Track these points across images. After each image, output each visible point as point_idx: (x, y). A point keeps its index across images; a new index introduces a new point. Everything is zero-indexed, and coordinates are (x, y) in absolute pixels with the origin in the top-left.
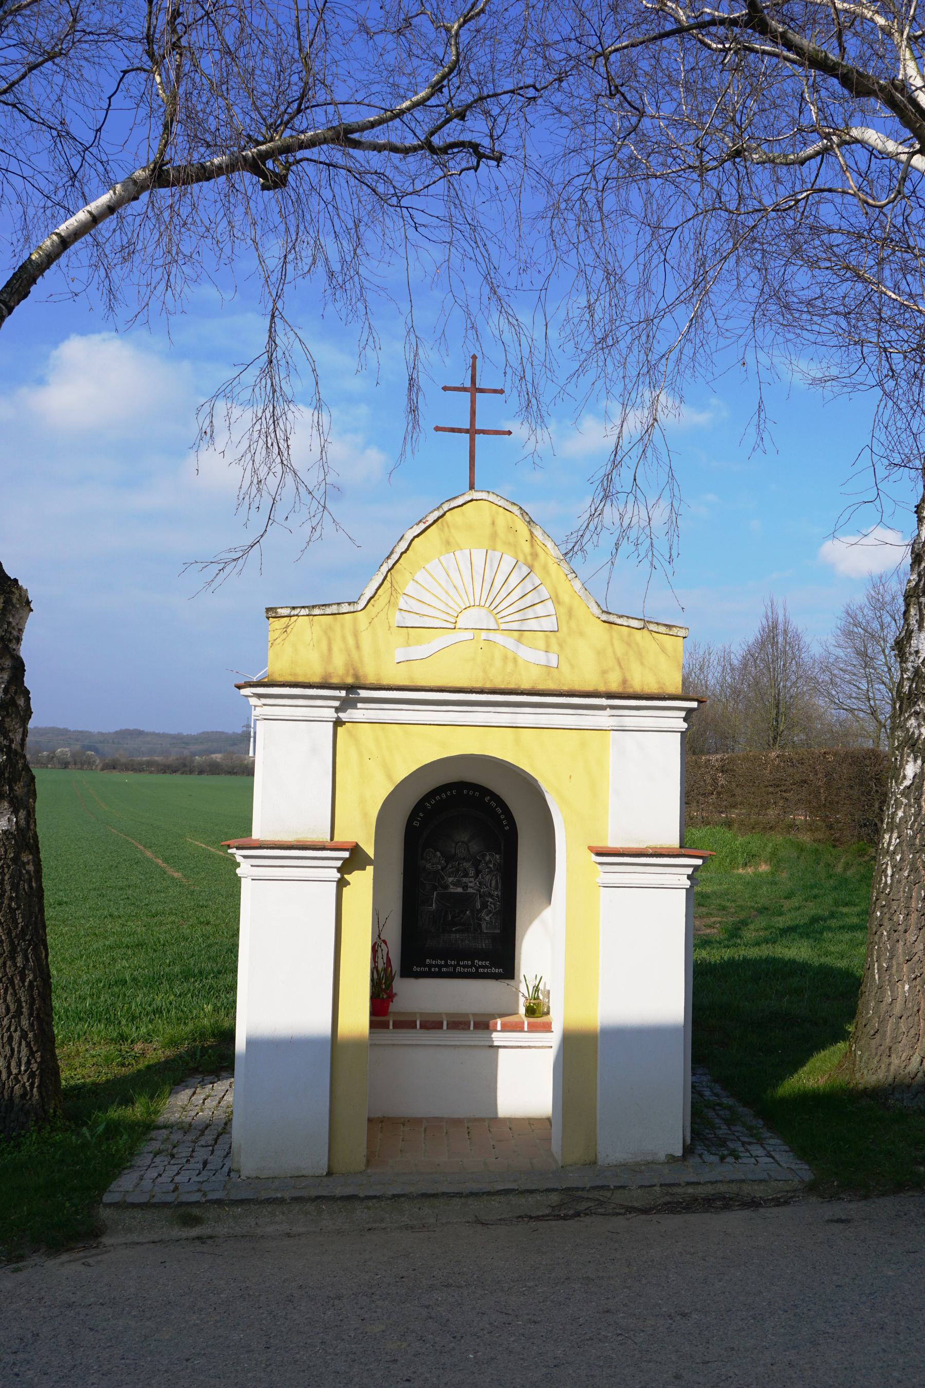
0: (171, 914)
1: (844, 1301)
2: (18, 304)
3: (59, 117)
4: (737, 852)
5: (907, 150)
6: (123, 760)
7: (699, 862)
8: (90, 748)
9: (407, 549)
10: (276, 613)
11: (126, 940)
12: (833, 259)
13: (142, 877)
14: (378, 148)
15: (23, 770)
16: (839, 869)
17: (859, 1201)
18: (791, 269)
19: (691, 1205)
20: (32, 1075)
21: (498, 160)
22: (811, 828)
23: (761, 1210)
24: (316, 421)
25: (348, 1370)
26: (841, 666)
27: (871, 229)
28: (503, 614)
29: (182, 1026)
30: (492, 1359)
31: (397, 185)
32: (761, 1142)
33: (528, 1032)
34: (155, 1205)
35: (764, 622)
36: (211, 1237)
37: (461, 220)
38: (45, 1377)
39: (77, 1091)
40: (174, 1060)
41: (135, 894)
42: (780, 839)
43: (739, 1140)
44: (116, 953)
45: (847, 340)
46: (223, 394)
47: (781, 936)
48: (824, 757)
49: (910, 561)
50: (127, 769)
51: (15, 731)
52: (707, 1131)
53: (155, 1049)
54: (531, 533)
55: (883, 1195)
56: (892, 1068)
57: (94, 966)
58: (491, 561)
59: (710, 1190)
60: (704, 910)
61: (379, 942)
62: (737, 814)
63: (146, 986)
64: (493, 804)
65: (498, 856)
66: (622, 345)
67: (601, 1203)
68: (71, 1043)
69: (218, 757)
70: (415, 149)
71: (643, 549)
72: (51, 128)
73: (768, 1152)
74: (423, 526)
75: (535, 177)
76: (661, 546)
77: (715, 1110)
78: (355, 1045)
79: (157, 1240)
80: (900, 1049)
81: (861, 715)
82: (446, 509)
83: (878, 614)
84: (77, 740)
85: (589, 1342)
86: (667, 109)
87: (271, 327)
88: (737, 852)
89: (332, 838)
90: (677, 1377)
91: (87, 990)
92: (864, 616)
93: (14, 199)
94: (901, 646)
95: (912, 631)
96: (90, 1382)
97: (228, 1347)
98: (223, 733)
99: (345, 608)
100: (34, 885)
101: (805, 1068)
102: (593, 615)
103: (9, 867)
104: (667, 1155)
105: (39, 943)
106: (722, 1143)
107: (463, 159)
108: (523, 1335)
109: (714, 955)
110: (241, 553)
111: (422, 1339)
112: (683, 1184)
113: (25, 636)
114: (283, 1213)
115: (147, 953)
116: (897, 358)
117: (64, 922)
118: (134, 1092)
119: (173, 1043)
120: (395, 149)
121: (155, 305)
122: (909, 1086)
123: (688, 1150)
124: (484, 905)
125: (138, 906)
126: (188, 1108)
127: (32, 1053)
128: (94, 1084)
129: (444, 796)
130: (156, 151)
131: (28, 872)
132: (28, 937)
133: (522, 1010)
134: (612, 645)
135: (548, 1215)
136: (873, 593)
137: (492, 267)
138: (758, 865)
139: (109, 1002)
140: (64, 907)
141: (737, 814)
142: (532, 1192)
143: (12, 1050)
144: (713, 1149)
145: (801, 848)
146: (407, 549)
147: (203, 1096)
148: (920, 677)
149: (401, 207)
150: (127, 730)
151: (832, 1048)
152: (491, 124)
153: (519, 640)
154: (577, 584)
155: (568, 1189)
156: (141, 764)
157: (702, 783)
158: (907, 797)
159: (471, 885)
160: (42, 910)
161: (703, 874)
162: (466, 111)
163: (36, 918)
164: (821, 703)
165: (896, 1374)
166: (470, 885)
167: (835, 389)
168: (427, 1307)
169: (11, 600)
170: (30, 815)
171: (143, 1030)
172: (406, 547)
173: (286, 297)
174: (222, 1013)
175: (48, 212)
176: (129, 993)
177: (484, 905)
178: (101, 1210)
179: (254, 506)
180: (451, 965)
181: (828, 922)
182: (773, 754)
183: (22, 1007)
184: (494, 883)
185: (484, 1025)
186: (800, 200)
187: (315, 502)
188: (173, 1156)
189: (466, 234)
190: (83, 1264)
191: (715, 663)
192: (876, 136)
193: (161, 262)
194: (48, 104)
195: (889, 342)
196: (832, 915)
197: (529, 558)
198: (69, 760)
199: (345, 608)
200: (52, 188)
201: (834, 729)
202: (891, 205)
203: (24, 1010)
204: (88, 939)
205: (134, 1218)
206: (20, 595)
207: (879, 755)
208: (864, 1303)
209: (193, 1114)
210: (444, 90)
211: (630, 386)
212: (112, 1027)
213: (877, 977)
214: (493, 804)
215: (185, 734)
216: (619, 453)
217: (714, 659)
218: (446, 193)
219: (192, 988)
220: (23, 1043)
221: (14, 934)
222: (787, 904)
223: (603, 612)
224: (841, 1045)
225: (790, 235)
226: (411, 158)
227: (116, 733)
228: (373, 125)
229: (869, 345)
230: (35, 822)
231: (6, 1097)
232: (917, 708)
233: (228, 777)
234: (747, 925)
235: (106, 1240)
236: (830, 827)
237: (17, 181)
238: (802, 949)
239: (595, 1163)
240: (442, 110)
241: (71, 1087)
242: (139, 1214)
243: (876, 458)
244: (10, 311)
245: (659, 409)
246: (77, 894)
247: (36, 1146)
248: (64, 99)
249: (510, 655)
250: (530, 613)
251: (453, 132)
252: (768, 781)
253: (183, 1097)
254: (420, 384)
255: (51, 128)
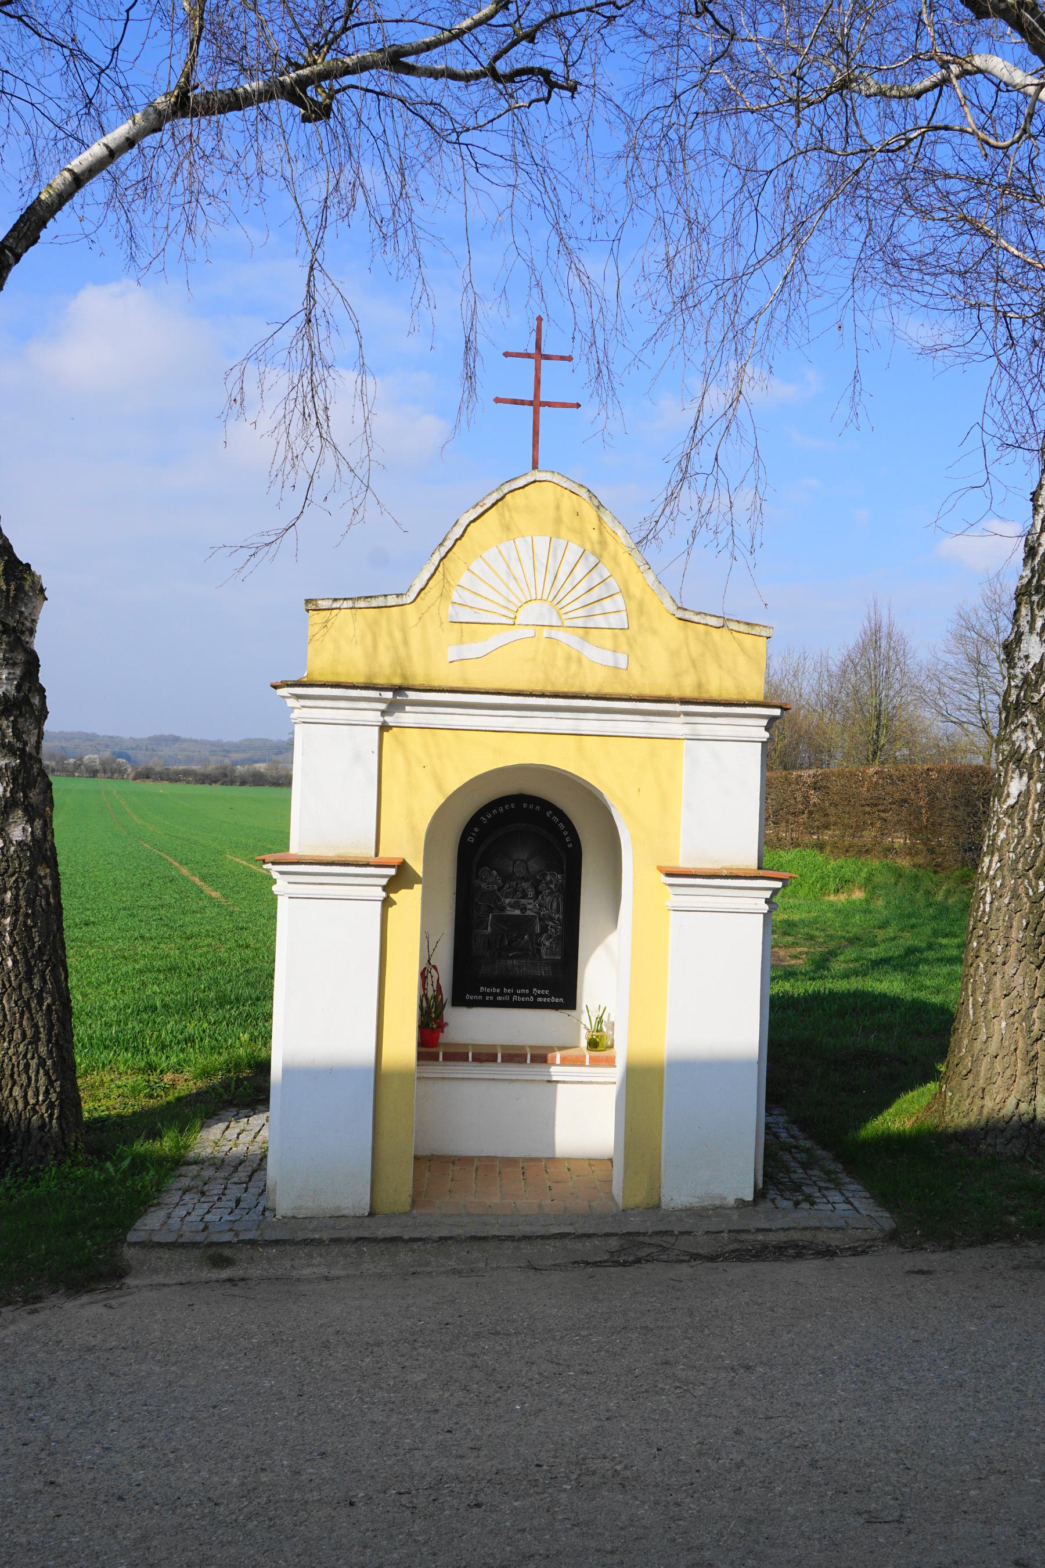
0: (207, 936)
1: (922, 1356)
2: (26, 250)
3: (69, 31)
4: (829, 877)
5: (1036, 81)
6: (158, 769)
7: (778, 885)
8: (121, 755)
9: (462, 535)
10: (316, 605)
11: (157, 964)
12: (950, 208)
13: (177, 896)
14: (434, 74)
15: (38, 775)
16: (940, 897)
17: (943, 1251)
18: (903, 220)
19: (759, 1253)
20: (51, 1106)
21: (573, 89)
22: (911, 852)
23: (836, 1259)
24: (359, 389)
25: (385, 1420)
26: (951, 673)
27: (993, 175)
28: (567, 609)
29: (216, 1056)
30: (540, 1410)
31: (459, 119)
32: (839, 1187)
33: (561, 1065)
34: (184, 1245)
35: (866, 623)
36: (243, 1279)
37: (529, 161)
38: (62, 1423)
39: (101, 1124)
40: (206, 1092)
41: (169, 915)
42: (876, 863)
43: (816, 1185)
44: (148, 977)
45: (962, 303)
46: (255, 356)
47: (873, 969)
48: (928, 774)
49: (1023, 555)
50: (162, 779)
51: (29, 732)
52: (782, 1175)
53: (186, 1080)
54: (600, 519)
55: (970, 1246)
56: (985, 1111)
57: (122, 991)
58: (555, 549)
59: (782, 1237)
60: (790, 939)
61: (429, 968)
62: (830, 836)
63: (178, 1013)
64: (555, 819)
65: (559, 876)
66: (705, 306)
67: (664, 1249)
68: (95, 1073)
69: (261, 767)
70: (477, 76)
71: (723, 538)
72: (63, 46)
73: (847, 1198)
74: (480, 510)
75: (613, 110)
76: (743, 532)
77: (790, 1152)
78: (401, 1075)
79: (184, 1282)
80: (994, 1091)
81: (971, 728)
82: (506, 491)
83: (994, 617)
84: (107, 746)
85: (645, 1395)
86: (766, 31)
87: (309, 281)
88: (829, 877)
89: (377, 854)
90: (738, 1432)
91: (113, 1016)
92: (978, 619)
93: (22, 130)
94: (1010, 649)
95: (1022, 634)
96: (109, 1429)
97: (259, 1394)
98: (267, 740)
99: (392, 600)
100: (52, 901)
101: (891, 1110)
102: (667, 611)
103: (24, 881)
104: (737, 1200)
105: (58, 964)
106: (797, 1187)
107: (532, 88)
108: (574, 1386)
109: (787, 987)
110: (275, 538)
111: (466, 1389)
112: (753, 1230)
113: (39, 627)
114: (321, 1255)
115: (180, 978)
116: (1017, 324)
117: (90, 943)
118: (163, 1125)
119: (205, 1073)
120: (454, 76)
121: (173, 248)
122: (1003, 1131)
123: (760, 1195)
124: (544, 929)
125: (172, 927)
126: (220, 1143)
127: (50, 1082)
128: (119, 1116)
129: (501, 810)
130: (179, 72)
131: (45, 887)
132: (45, 958)
133: (584, 1043)
134: (687, 645)
135: (606, 1261)
136: (989, 594)
137: (562, 216)
138: (851, 892)
139: (137, 1029)
140: (91, 927)
141: (830, 836)
142: (589, 1236)
143: (29, 1078)
144: (787, 1194)
145: (899, 874)
146: (462, 535)
147: (238, 1131)
148: (1029, 685)
149: (460, 144)
150: (162, 736)
151: (922, 1089)
152: (565, 48)
153: (585, 638)
154: (651, 577)
155: (629, 1234)
156: (177, 773)
157: (792, 801)
158: (1010, 817)
159: (530, 907)
160: (61, 929)
161: (791, 900)
162: (535, 31)
163: (55, 937)
164: (927, 715)
165: (973, 1434)
166: (529, 907)
167: (947, 360)
168: (473, 1355)
169: (23, 587)
170: (47, 825)
171: (174, 1059)
172: (461, 533)
173: (326, 247)
174: (260, 1042)
175: (60, 145)
176: (158, 1020)
177: (544, 929)
178: (125, 1249)
179: (289, 484)
180: (507, 994)
181: (925, 954)
182: (871, 771)
183: (40, 1033)
184: (555, 905)
185: (541, 1058)
186: (911, 140)
187: (357, 482)
188: (203, 1193)
189: (533, 176)
190: (105, 1306)
191: (811, 669)
192: (1002, 65)
193: (180, 200)
194: (56, 16)
195: (1009, 305)
196: (930, 947)
197: (597, 547)
198: (99, 767)
199: (392, 600)
200: (65, 116)
201: (941, 744)
202: (1015, 146)
203: (42, 1036)
204: (117, 962)
205: (161, 1258)
206: (33, 582)
207: (988, 773)
208: (942, 1359)
209: (226, 1149)
210: (510, 6)
211: (713, 353)
212: (140, 1056)
213: (971, 1012)
214: (555, 819)
215: (225, 741)
216: (699, 428)
217: (809, 664)
218: (511, 128)
219: (227, 1016)
220: (41, 1071)
221: (30, 954)
222: (881, 934)
223: (679, 608)
224: (932, 1086)
225: (900, 180)
226: (474, 87)
227: (150, 739)
228: (428, 47)
229: (987, 308)
230: (52, 833)
231: (23, 1129)
232: (1025, 719)
233: (274, 789)
234: (836, 956)
235: (130, 1281)
236: (932, 851)
237: (25, 109)
238: (895, 983)
239: (658, 1206)
240: (509, 30)
241: (95, 1119)
242: (166, 1255)
243: (986, 438)
244: (17, 259)
245: (746, 379)
246: (106, 913)
247: (55, 1182)
248: (73, 9)
249: (574, 654)
250: (597, 609)
251: (521, 56)
252: (865, 800)
253: (216, 1131)
254: (478, 347)
255: (63, 46)
